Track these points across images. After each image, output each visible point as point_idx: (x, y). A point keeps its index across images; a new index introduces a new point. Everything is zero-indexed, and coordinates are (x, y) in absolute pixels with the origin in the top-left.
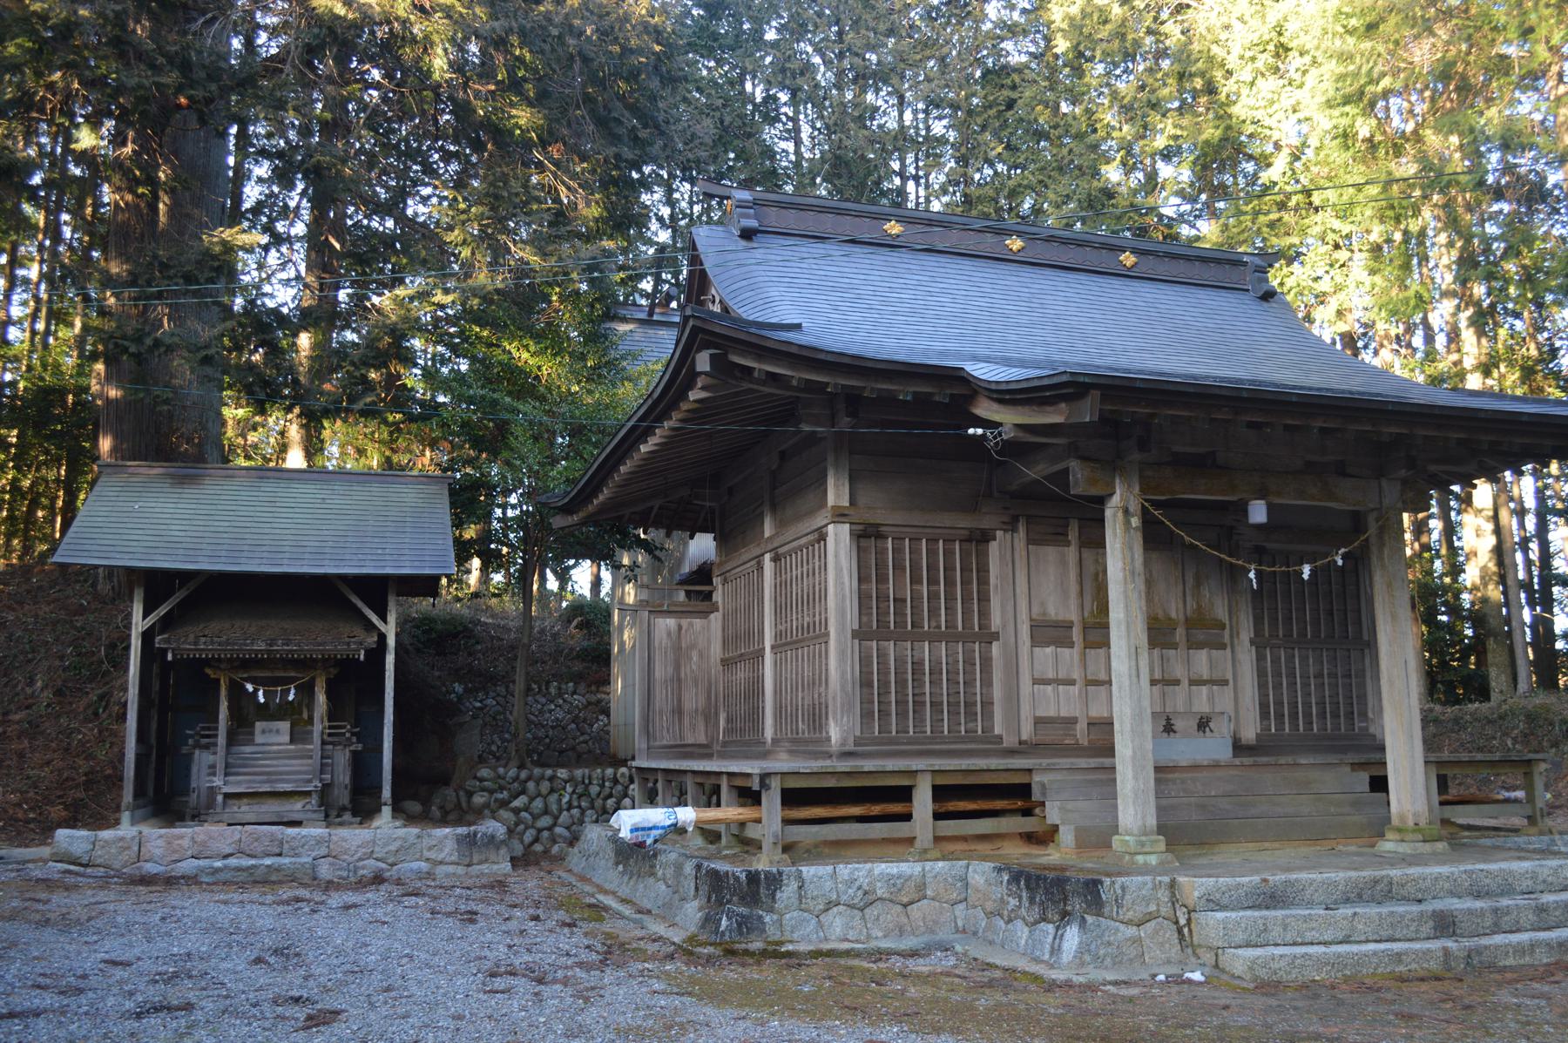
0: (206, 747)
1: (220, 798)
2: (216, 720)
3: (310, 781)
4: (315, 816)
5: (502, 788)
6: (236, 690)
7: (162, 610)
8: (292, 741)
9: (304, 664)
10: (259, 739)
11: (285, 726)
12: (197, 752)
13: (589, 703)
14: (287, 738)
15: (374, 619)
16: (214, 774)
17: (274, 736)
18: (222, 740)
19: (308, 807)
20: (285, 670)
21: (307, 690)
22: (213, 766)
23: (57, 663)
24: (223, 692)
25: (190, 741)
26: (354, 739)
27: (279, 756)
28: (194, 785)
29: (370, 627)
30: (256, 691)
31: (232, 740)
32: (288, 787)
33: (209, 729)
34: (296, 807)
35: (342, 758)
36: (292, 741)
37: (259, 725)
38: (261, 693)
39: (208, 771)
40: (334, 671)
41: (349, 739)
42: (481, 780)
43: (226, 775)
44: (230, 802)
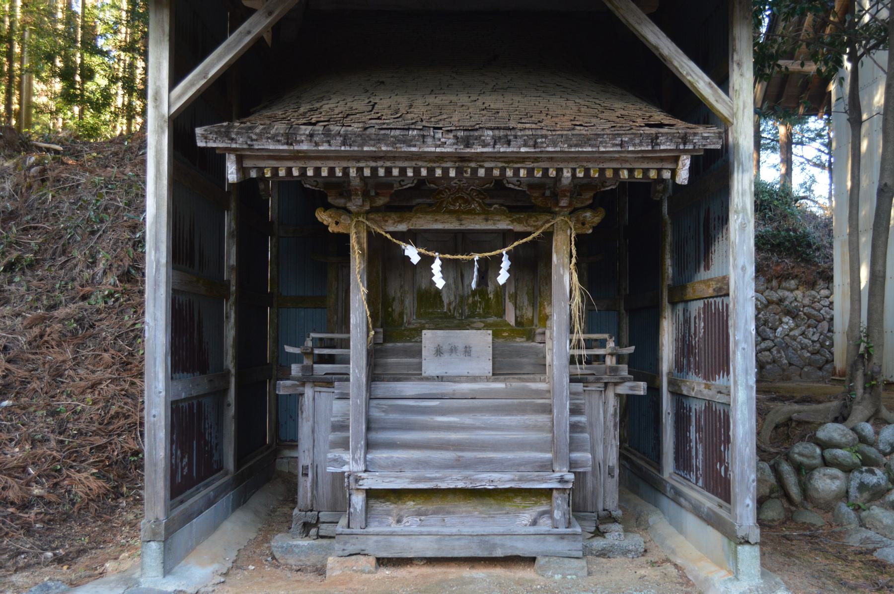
0: (327, 382)
1: (358, 500)
2: (344, 324)
3: (547, 466)
4: (563, 547)
5: (868, 463)
6: (384, 257)
7: (214, 64)
8: (497, 373)
9: (530, 198)
10: (430, 367)
11: (480, 339)
12: (308, 391)
13: (770, 302)
14: (486, 367)
15: (700, 81)
16: (344, 445)
17: (457, 358)
18: (357, 368)
19: (545, 525)
20: (487, 214)
21: (533, 264)
22: (341, 427)
23: (127, 235)
24: (357, 265)
25: (295, 369)
26: (624, 370)
27: (473, 403)
28: (304, 459)
29: (695, 110)
30: (427, 261)
31: (374, 375)
32: (503, 480)
33: (332, 344)
34: (517, 527)
35: (603, 411)
36: (497, 373)
37: (430, 338)
38: (436, 267)
39: (330, 427)
40: (592, 218)
41: (614, 370)
42: (824, 445)
43: (370, 446)
44: (380, 507)
